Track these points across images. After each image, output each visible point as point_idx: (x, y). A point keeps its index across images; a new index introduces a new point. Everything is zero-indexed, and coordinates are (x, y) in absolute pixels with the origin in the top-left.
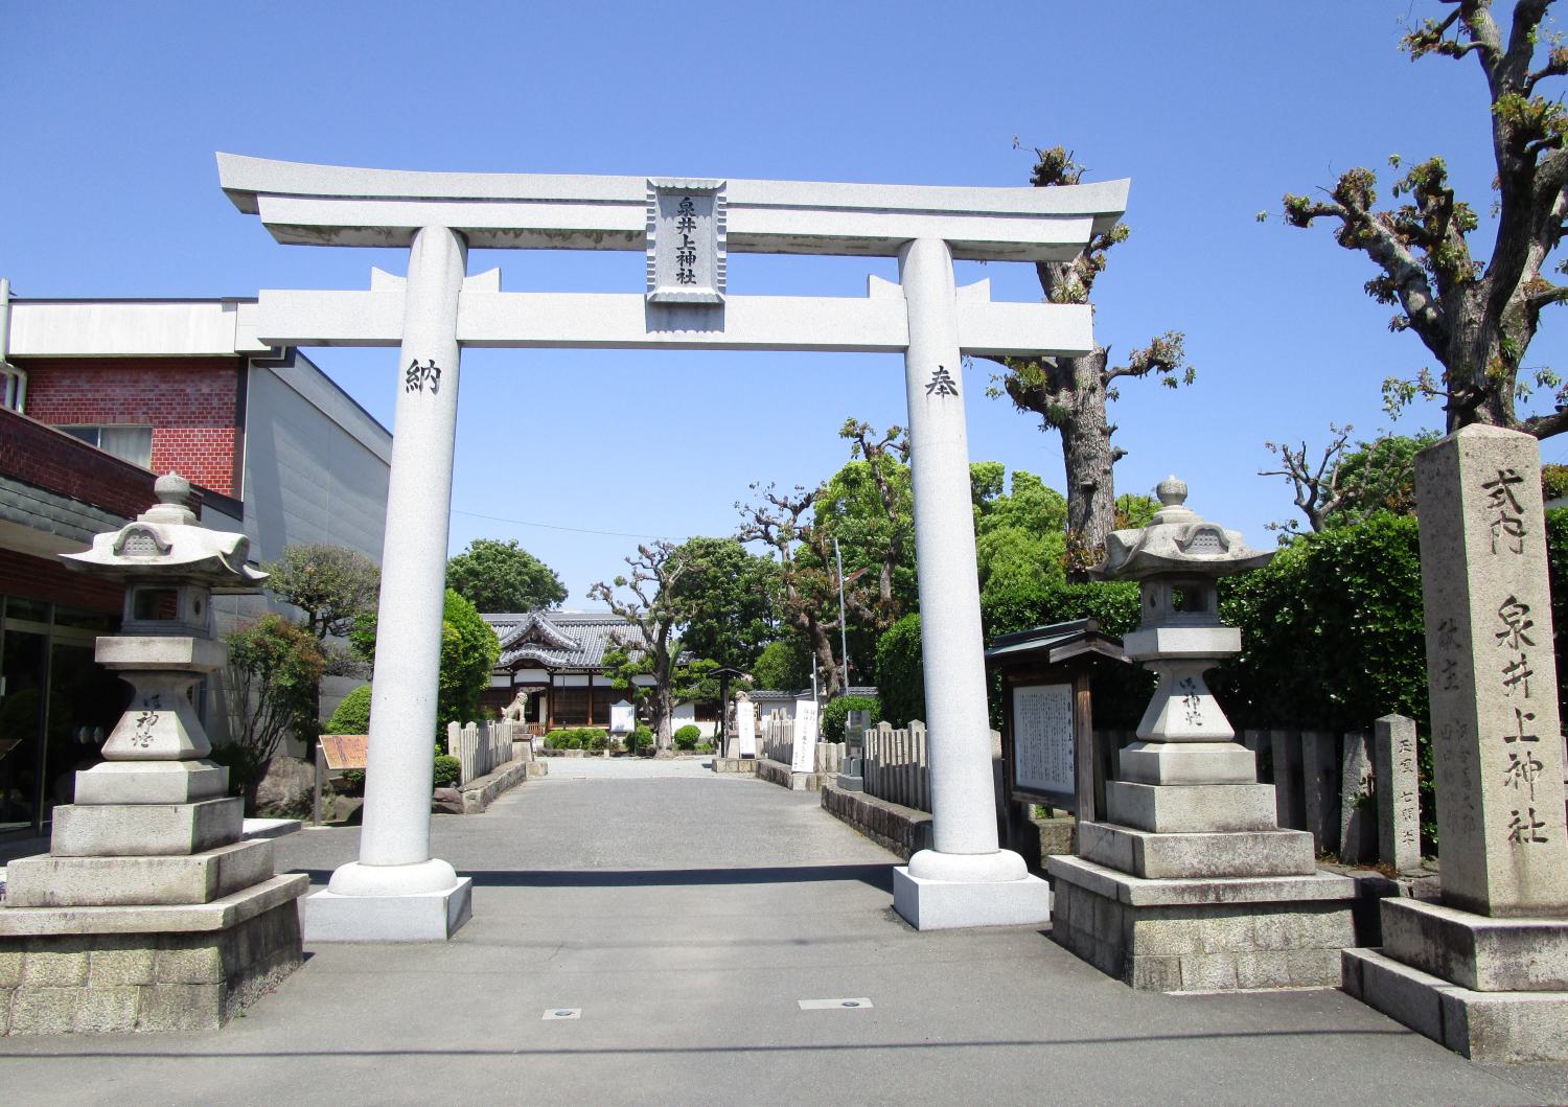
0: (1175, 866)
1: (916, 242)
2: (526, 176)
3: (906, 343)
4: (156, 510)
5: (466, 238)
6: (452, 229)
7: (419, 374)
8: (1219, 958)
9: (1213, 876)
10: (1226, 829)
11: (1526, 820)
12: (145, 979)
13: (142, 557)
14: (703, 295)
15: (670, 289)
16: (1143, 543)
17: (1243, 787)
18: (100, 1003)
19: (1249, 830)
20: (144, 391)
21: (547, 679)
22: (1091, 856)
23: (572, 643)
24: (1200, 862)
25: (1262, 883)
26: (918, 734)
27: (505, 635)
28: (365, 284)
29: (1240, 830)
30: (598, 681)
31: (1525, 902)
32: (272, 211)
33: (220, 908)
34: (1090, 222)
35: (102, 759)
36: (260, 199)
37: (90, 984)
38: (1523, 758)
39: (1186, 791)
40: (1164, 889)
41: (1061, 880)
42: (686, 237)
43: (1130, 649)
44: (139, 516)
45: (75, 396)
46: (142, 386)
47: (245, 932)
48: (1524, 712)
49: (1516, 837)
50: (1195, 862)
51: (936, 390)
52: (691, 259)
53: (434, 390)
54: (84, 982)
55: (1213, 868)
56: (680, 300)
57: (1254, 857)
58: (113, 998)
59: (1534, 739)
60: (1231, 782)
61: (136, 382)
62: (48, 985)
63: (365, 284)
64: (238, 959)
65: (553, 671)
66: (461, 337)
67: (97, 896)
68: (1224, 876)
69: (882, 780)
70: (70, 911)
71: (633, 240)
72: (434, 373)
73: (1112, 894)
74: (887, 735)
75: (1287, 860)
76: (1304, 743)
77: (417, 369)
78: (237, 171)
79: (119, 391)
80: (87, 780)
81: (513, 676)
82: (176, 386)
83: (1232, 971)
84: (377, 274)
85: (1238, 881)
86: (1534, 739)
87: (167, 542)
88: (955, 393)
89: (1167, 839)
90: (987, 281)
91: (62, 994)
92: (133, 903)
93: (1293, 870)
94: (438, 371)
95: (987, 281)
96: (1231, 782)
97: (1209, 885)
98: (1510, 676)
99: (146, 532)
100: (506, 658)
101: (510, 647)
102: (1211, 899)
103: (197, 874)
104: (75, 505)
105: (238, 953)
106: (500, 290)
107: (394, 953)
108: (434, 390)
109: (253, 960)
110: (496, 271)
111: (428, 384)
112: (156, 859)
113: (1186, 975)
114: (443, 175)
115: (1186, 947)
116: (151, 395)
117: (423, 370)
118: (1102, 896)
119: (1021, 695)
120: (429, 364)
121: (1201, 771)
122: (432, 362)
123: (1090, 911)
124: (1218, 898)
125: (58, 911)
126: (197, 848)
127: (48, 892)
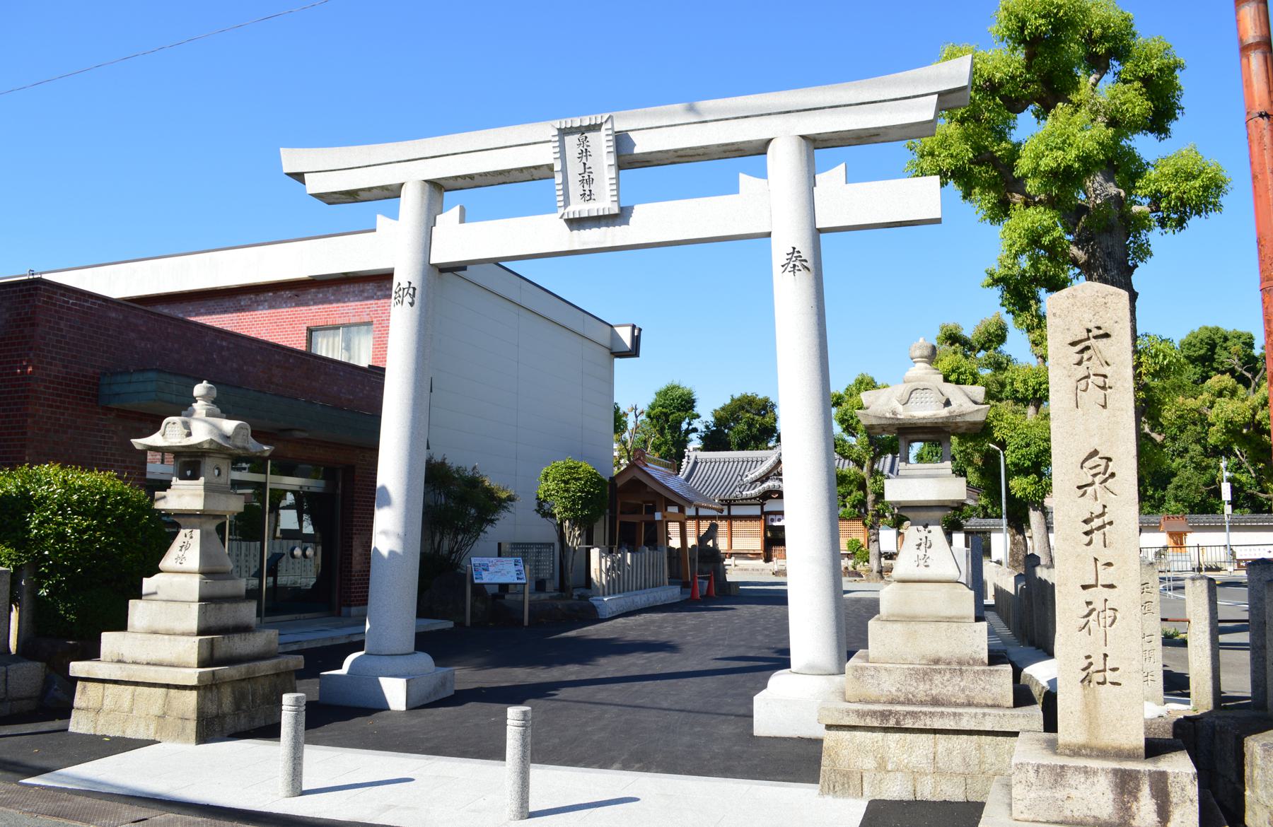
0: (873, 692)
2: (492, 131)
5: (814, 143)
6: (803, 137)
8: (899, 775)
11: (1098, 664)
12: (160, 713)
15: (579, 208)
24: (898, 690)
28: (733, 189)
31: (1094, 743)
32: (315, 184)
38: (1099, 605)
48: (1102, 561)
49: (1086, 680)
50: (893, 690)
52: (590, 181)
57: (950, 688)
59: (1111, 586)
60: (949, 620)
61: (363, 291)
63: (733, 189)
67: (143, 657)
71: (540, 173)
72: (411, 291)
78: (292, 160)
80: (148, 584)
81: (762, 505)
84: (743, 178)
86: (1111, 586)
90: (379, 217)
93: (990, 702)
95: (379, 217)
98: (1088, 528)
102: (892, 723)
106: (374, 230)
110: (843, 166)
111: (408, 299)
114: (757, 96)
115: (869, 763)
121: (919, 608)
124: (898, 722)
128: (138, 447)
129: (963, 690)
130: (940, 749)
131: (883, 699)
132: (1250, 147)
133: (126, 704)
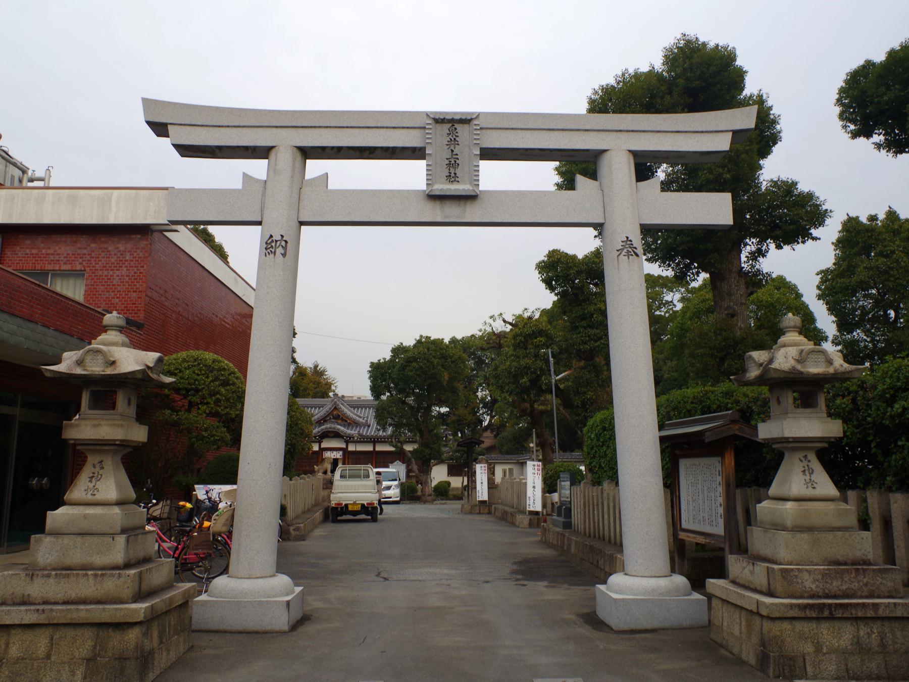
1: (608, 153)
3: (601, 221)
4: (103, 337)
6: (630, 151)
7: (273, 244)
8: (833, 657)
9: (827, 596)
10: (838, 563)
13: (96, 368)
14: (464, 190)
16: (771, 361)
17: (847, 534)
18: (59, 672)
19: (853, 564)
20: (80, 248)
21: (344, 446)
22: (737, 581)
23: (361, 420)
24: (817, 586)
25: (864, 604)
26: (608, 495)
27: (318, 414)
29: (846, 564)
30: (380, 448)
33: (142, 606)
34: (729, 136)
35: (63, 503)
36: (170, 127)
37: (53, 658)
39: (805, 536)
40: (792, 606)
41: (717, 597)
42: (452, 151)
43: (766, 431)
44: (93, 341)
45: (34, 251)
46: (79, 245)
47: (156, 623)
50: (813, 587)
51: (624, 253)
53: (284, 255)
54: (48, 656)
55: (827, 591)
56: (448, 193)
58: (67, 669)
60: (839, 529)
61: (76, 242)
62: (23, 659)
64: (151, 641)
65: (349, 440)
66: (301, 219)
68: (835, 597)
69: (585, 521)
70: (41, 607)
72: (283, 243)
73: (754, 608)
74: (611, 498)
75: (882, 586)
76: (892, 502)
77: (272, 241)
79: (63, 249)
80: (57, 517)
82: (102, 245)
83: (843, 667)
85: (846, 601)
87: (112, 359)
88: (637, 255)
89: (792, 570)
91: (33, 665)
92: (84, 602)
94: (286, 242)
96: (839, 529)
97: (824, 604)
99: (98, 351)
100: (316, 430)
101: (320, 422)
103: (126, 582)
104: (40, 328)
105: (152, 637)
107: (251, 639)
108: (284, 255)
109: (161, 642)
111: (280, 251)
112: (100, 572)
113: (809, 669)
115: (809, 648)
116: (85, 251)
117: (276, 241)
118: (747, 610)
119: (685, 466)
120: (279, 238)
122: (282, 236)
123: (738, 620)
125: (32, 607)
126: (127, 566)
127: (26, 594)
128: (48, 375)
129: (866, 585)
130: (862, 633)
131: (806, 595)
132: (673, 511)
133: (42, 650)
